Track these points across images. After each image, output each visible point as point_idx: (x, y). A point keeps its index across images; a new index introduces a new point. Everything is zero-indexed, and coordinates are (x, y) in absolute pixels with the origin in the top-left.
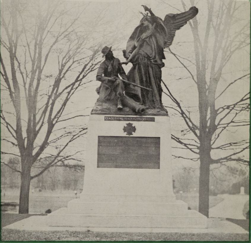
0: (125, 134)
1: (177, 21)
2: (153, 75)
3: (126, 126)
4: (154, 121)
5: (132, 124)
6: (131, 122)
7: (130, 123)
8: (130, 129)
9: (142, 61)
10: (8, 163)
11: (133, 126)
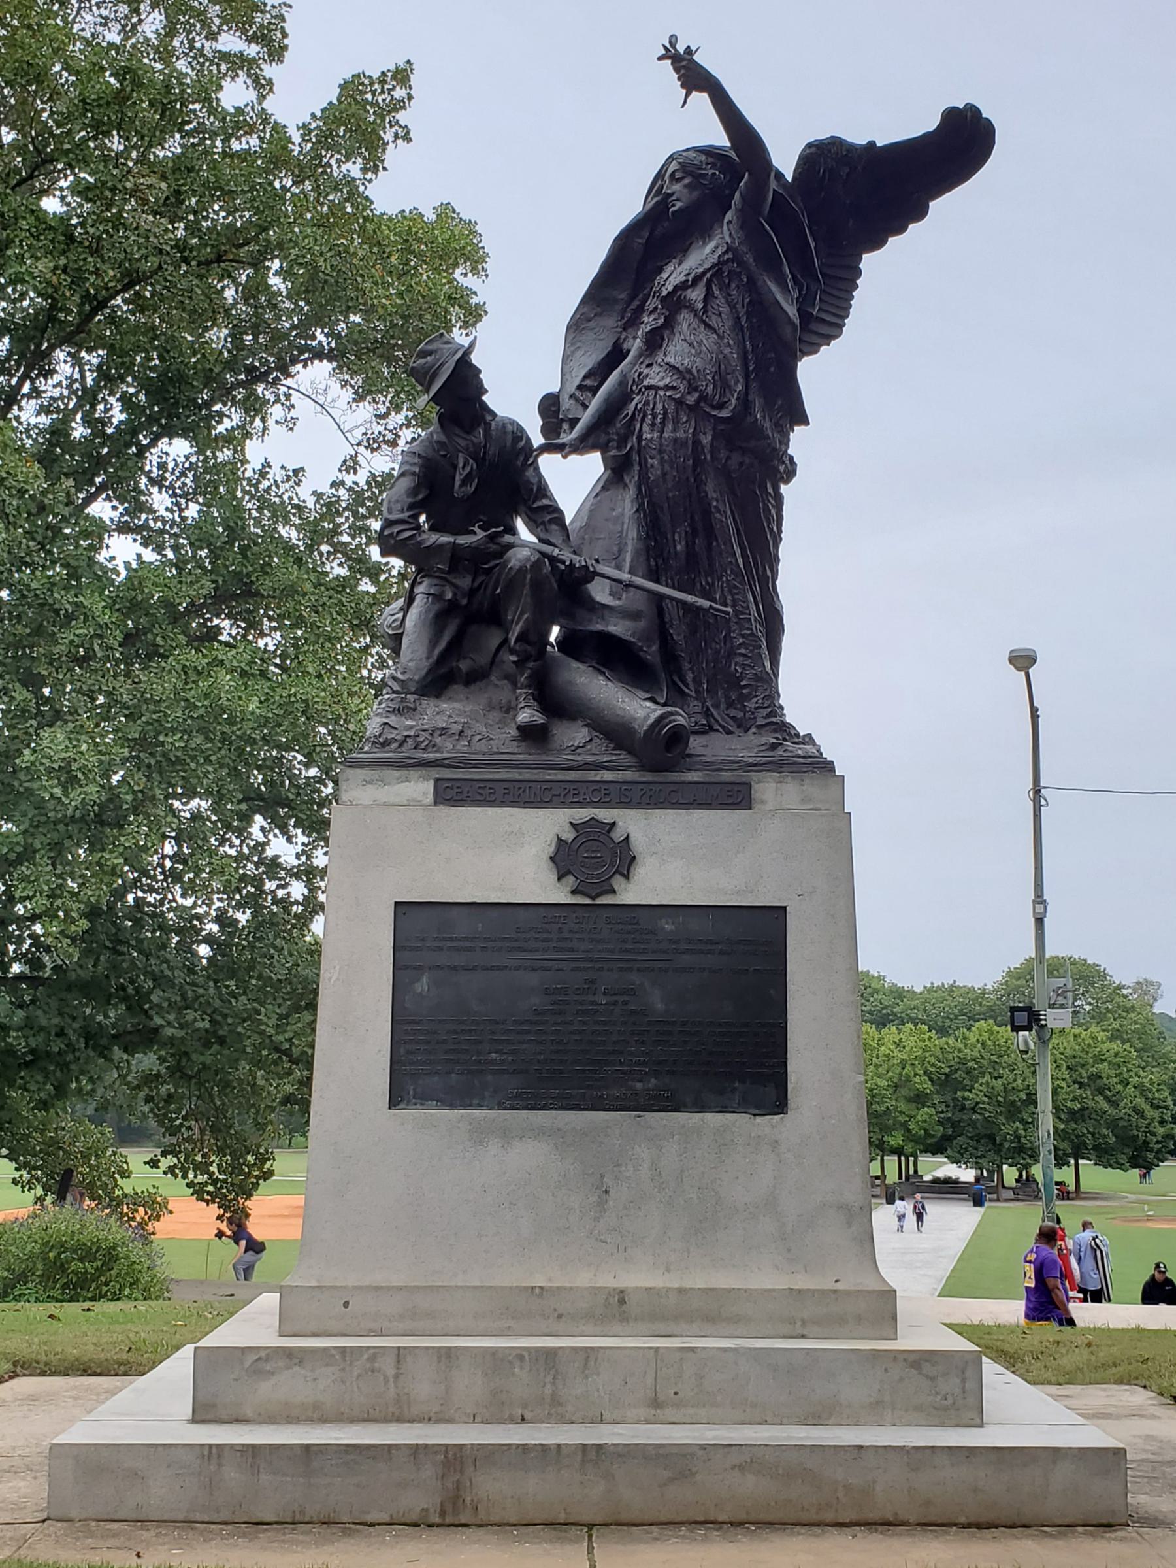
0: (559, 894)
3: (569, 835)
6: (604, 814)
9: (662, 432)
10: (1037, 1198)
11: (618, 835)
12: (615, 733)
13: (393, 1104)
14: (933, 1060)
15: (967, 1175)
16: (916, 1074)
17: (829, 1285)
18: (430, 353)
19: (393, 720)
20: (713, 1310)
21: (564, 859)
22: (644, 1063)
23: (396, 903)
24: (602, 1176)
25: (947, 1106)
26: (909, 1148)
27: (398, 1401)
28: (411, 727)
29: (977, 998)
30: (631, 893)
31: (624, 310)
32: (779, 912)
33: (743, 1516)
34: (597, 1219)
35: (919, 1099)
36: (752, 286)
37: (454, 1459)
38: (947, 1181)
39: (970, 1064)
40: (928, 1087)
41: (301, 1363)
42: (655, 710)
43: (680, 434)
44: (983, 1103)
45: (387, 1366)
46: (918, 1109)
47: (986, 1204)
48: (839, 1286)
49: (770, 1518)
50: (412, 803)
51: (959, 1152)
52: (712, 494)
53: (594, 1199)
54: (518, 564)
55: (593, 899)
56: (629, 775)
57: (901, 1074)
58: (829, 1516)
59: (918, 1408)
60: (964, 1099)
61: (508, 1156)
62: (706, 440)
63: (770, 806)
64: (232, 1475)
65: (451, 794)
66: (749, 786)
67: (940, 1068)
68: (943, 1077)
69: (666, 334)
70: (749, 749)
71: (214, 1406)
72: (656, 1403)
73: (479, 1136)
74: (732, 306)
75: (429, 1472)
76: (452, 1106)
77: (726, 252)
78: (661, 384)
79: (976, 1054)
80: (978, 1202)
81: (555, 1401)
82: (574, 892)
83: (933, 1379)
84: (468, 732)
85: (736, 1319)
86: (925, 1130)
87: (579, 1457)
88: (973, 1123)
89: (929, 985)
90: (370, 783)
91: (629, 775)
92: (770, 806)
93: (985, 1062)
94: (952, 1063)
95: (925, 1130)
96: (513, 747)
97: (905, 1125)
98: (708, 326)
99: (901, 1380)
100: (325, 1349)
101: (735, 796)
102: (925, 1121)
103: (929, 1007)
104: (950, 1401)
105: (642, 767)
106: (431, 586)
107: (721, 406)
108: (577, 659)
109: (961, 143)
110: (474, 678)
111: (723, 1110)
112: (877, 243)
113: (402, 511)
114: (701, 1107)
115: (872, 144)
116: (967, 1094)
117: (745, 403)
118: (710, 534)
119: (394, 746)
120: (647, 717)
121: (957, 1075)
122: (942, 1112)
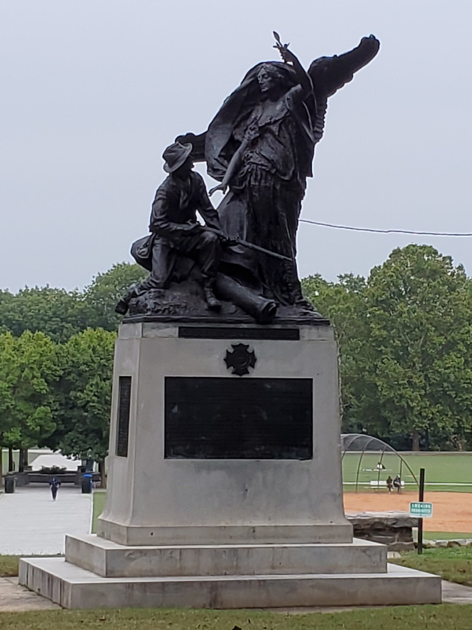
0: (227, 374)
1: (337, 71)
2: (291, 140)
3: (231, 351)
4: (297, 338)
5: (248, 346)
6: (244, 342)
7: (241, 345)
8: (240, 359)
11: (250, 350)
12: (248, 309)
13: (166, 457)
14: (49, 364)
15: (72, 464)
16: (34, 377)
19: (157, 301)
20: (287, 534)
21: (230, 360)
24: (245, 484)
25: (61, 405)
26: (25, 442)
27: (181, 568)
28: (166, 304)
29: (70, 302)
30: (254, 373)
35: (36, 399)
36: (298, 127)
37: (214, 586)
38: (55, 471)
39: (83, 367)
40: (44, 387)
41: (145, 555)
42: (265, 301)
43: (268, 184)
44: (93, 402)
45: (177, 555)
46: (36, 408)
47: (93, 491)
48: (332, 524)
51: (70, 445)
52: (279, 209)
53: (242, 492)
54: (210, 240)
56: (254, 326)
57: (20, 377)
58: (342, 603)
60: (76, 398)
61: (208, 476)
62: (278, 187)
63: (306, 338)
64: (137, 593)
66: (298, 330)
67: (56, 370)
68: (58, 379)
69: (259, 140)
70: (295, 314)
72: (273, 567)
73: (199, 469)
74: (289, 134)
75: (205, 591)
76: (188, 457)
77: (287, 113)
78: (260, 163)
79: (87, 358)
80: (86, 489)
81: (237, 567)
82: (233, 373)
83: (369, 556)
84: (188, 307)
85: (294, 537)
86: (41, 426)
87: (258, 584)
88: (83, 420)
89: (24, 289)
91: (254, 326)
92: (306, 338)
93: (95, 366)
94: (66, 366)
95: (41, 426)
96: (207, 313)
97: (22, 423)
102: (41, 419)
103: (25, 309)
104: (375, 564)
105: (258, 322)
106: (163, 241)
107: (285, 175)
108: (227, 275)
109: (369, 48)
110: (182, 280)
112: (332, 91)
114: (281, 457)
115: (335, 56)
116: (79, 394)
117: (294, 174)
118: (277, 223)
119: (161, 312)
120: (262, 305)
121: (70, 378)
122: (56, 410)
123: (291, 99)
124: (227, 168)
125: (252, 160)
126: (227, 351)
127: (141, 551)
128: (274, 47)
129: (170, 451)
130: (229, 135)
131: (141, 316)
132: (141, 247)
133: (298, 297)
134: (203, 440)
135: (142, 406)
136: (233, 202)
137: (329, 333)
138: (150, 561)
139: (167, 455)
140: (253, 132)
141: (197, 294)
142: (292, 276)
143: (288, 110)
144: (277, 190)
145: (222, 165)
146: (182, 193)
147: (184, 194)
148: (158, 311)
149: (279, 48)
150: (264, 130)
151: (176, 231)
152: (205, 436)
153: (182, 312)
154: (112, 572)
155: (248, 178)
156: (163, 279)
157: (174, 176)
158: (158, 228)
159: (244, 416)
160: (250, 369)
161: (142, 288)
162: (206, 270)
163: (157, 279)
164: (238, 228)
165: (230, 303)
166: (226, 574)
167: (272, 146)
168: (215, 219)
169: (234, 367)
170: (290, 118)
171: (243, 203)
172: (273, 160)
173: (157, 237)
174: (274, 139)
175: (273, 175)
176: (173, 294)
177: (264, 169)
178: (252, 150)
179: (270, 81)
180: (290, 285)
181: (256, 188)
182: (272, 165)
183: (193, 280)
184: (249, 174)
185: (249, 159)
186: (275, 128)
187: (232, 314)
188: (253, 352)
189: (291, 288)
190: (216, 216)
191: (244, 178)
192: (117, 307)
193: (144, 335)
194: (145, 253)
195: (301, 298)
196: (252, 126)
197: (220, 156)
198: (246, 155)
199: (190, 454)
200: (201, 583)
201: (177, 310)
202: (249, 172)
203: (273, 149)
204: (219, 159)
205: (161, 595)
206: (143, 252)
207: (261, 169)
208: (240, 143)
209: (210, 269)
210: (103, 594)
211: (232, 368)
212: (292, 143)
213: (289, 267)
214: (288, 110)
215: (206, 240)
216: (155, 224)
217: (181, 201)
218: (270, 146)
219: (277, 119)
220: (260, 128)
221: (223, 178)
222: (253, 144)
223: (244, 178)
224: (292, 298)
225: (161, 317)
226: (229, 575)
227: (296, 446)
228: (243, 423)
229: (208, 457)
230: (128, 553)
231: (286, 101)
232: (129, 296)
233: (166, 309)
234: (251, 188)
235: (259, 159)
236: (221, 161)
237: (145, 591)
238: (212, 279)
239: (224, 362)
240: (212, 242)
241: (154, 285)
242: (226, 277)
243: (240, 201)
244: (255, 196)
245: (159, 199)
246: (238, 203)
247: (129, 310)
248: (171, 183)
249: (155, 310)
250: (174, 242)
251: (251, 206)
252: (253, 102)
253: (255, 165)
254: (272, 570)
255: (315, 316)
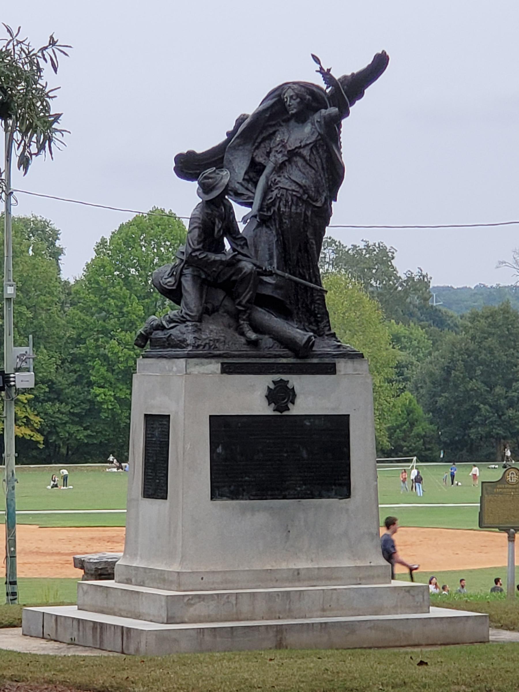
3: (272, 386)
6: (285, 377)
7: (281, 380)
8: (280, 396)
12: (288, 344)
13: (212, 499)
17: (369, 564)
18: (211, 178)
19: (196, 335)
20: (330, 575)
22: (300, 480)
23: (210, 416)
28: (205, 339)
30: (295, 410)
31: (255, 142)
32: (346, 418)
33: (371, 645)
34: (286, 542)
37: (279, 629)
41: (203, 600)
43: (299, 211)
45: (233, 599)
48: (372, 564)
49: (380, 645)
50: (213, 373)
52: (310, 237)
53: (285, 534)
54: (249, 271)
55: (281, 412)
58: (398, 644)
59: (409, 607)
61: (253, 517)
62: (309, 213)
63: (342, 373)
64: (207, 638)
65: (228, 369)
66: (335, 364)
70: (329, 347)
71: (174, 618)
72: (323, 610)
74: (320, 157)
75: (271, 634)
76: (232, 499)
78: (290, 188)
81: (290, 610)
83: (413, 596)
84: (227, 341)
85: (337, 579)
87: (319, 627)
90: (197, 365)
96: (245, 348)
98: (311, 166)
99: (403, 597)
100: (212, 595)
101: (330, 369)
104: (419, 604)
105: (297, 356)
106: (193, 271)
107: (316, 201)
108: (261, 307)
109: (380, 63)
111: (329, 497)
113: (198, 244)
114: (321, 497)
119: (202, 347)
123: (323, 122)
124: (254, 193)
125: (280, 185)
126: (268, 387)
127: (199, 596)
128: (317, 71)
129: (217, 491)
130: (251, 156)
131: (179, 352)
132: (166, 277)
133: (327, 328)
134: (246, 481)
135: (188, 446)
136: (260, 228)
137: (363, 367)
138: (208, 606)
139: (213, 497)
140: (280, 156)
141: (229, 327)
142: (321, 306)
143: (319, 134)
144: (308, 217)
145: (247, 189)
146: (217, 222)
147: (219, 222)
148: (198, 346)
149: (321, 73)
150: (293, 154)
151: (215, 261)
152: (249, 477)
153: (221, 347)
154: (173, 618)
155: (277, 204)
156: (198, 311)
157: (208, 204)
158: (196, 258)
159: (285, 455)
160: (290, 405)
161: (171, 321)
162: (244, 302)
163: (191, 312)
164: (267, 256)
165: (267, 336)
166: (279, 618)
167: (303, 170)
168: (246, 247)
169: (275, 404)
170: (321, 142)
171: (271, 230)
172: (305, 186)
173: (186, 266)
174: (304, 164)
175: (304, 201)
176: (209, 328)
177: (295, 195)
178: (280, 174)
179: (298, 103)
180: (319, 316)
181: (286, 214)
182: (304, 191)
183: (225, 312)
184: (278, 201)
185: (277, 184)
186: (306, 152)
187: (270, 348)
188: (293, 388)
189: (319, 319)
190: (246, 244)
191: (273, 204)
192: (137, 340)
193: (188, 371)
194: (172, 283)
195: (330, 329)
196: (279, 148)
197: (244, 179)
198: (273, 179)
199: (234, 496)
200: (267, 626)
201: (217, 345)
202: (278, 198)
203: (304, 174)
204: (243, 183)
205: (230, 640)
206: (169, 282)
207: (292, 195)
208: (263, 167)
209: (248, 301)
210: (176, 640)
211: (273, 404)
212: (323, 168)
213: (317, 297)
214: (319, 134)
215: (244, 271)
216: (193, 254)
217: (216, 230)
218: (300, 170)
219: (308, 142)
220: (289, 151)
221: (252, 203)
222: (280, 168)
223: (273, 204)
224: (321, 329)
225: (203, 352)
226: (283, 618)
227: (335, 485)
228: (281, 462)
229: (252, 497)
230: (186, 599)
231: (316, 124)
232: (150, 329)
233: (206, 343)
234: (280, 215)
235: (289, 183)
236: (246, 185)
237: (215, 636)
238: (248, 311)
239: (265, 398)
240: (251, 273)
241: (188, 318)
242: (260, 309)
243: (267, 227)
244: (285, 223)
245: (195, 228)
246: (264, 229)
247: (149, 342)
248: (206, 211)
249: (196, 345)
250: (205, 273)
251: (282, 234)
252: (274, 123)
253: (285, 191)
254: (322, 613)
255: (348, 349)
